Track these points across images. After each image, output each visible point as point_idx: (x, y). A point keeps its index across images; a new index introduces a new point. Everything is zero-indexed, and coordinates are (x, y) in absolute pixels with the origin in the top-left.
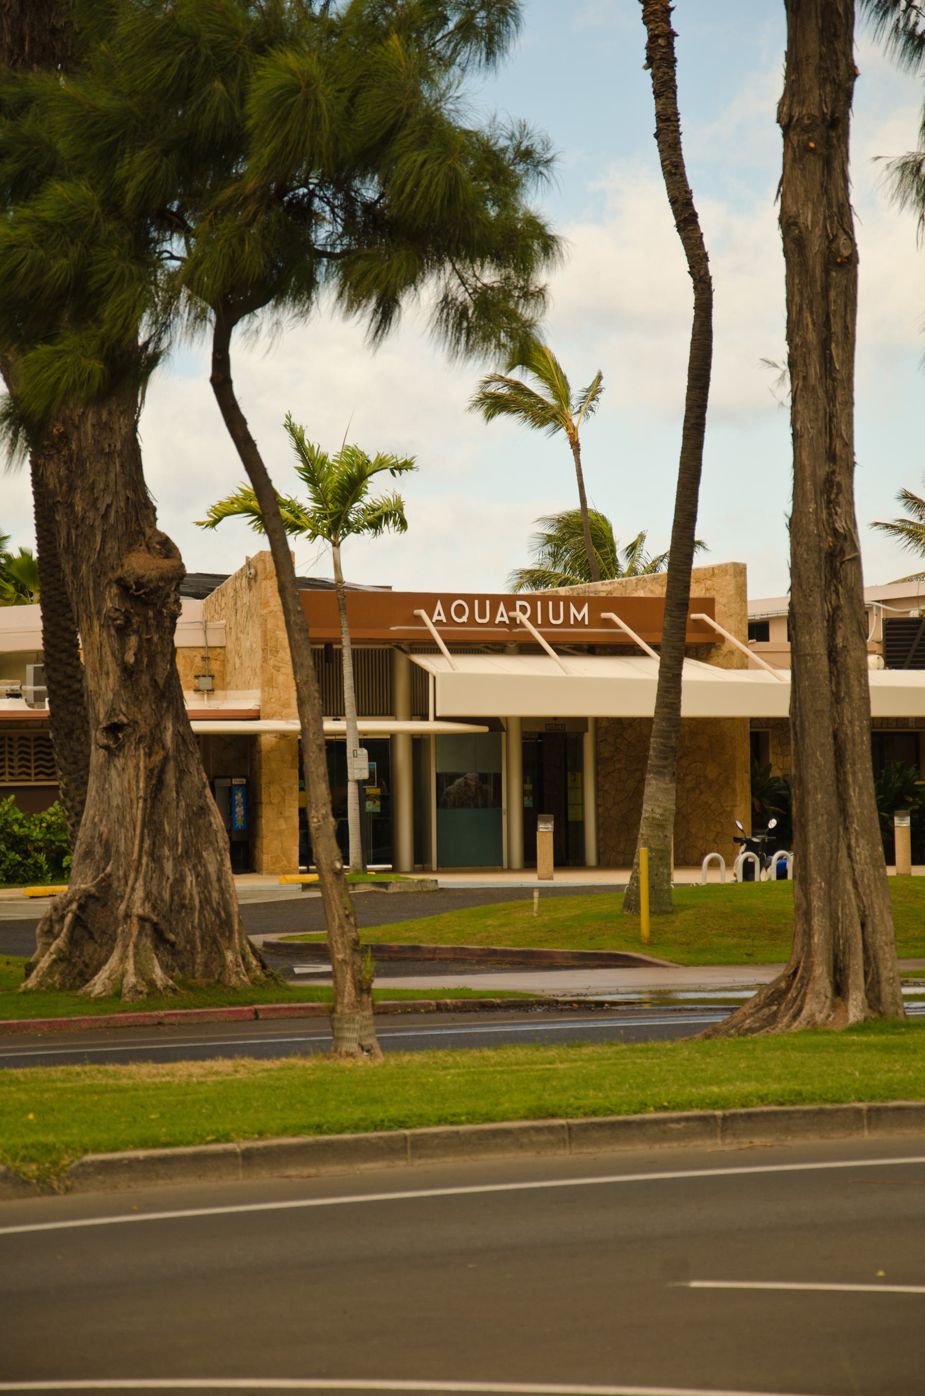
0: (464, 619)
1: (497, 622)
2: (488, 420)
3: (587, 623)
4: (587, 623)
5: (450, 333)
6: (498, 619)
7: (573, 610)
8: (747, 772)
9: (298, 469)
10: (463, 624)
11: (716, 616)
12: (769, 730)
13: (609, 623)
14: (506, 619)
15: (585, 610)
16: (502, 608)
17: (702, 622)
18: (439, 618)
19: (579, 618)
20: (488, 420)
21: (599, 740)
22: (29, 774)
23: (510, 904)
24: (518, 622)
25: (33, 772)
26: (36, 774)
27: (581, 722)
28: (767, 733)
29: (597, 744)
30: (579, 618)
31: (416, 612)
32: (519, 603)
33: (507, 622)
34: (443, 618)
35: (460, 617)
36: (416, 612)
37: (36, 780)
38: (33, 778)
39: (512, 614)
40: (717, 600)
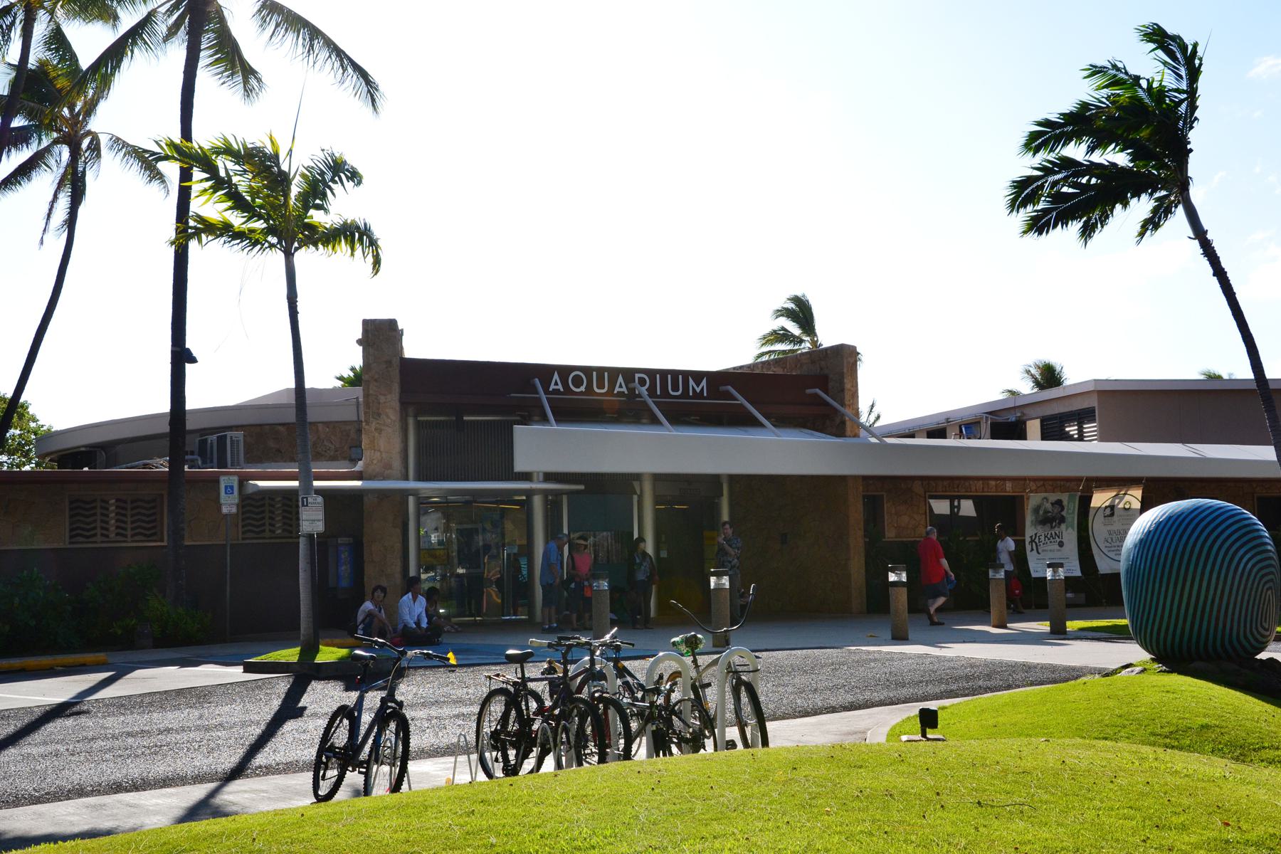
0: (582, 389)
1: (551, 389)
4: (705, 394)
5: (199, 151)
6: (617, 389)
7: (691, 382)
8: (860, 529)
9: (1087, 232)
10: (581, 393)
14: (624, 389)
15: (704, 383)
17: (816, 395)
19: (698, 390)
22: (126, 536)
23: (975, 697)
24: (637, 392)
25: (129, 533)
26: (133, 536)
27: (715, 480)
28: (883, 495)
30: (698, 390)
32: (637, 376)
33: (626, 392)
34: (560, 387)
35: (578, 387)
37: (133, 541)
38: (129, 539)
39: (631, 385)
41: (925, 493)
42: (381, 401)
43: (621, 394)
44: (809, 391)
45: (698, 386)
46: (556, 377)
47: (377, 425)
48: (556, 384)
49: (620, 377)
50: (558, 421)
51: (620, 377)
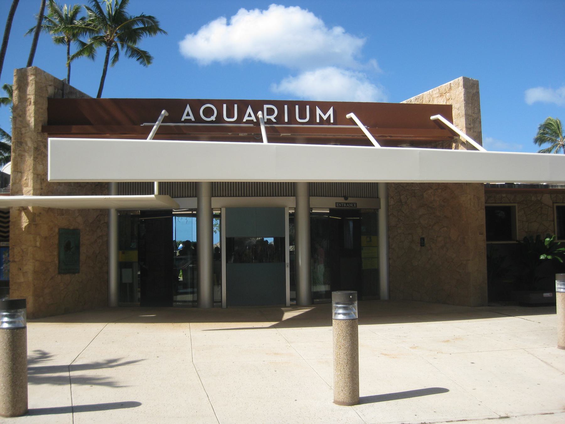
0: (213, 118)
2: (93, 58)
3: (332, 121)
4: (332, 121)
6: (246, 118)
7: (318, 111)
10: (212, 122)
11: (454, 121)
12: (516, 205)
13: (352, 121)
14: (253, 118)
15: (331, 112)
16: (249, 110)
18: (250, 118)
19: (325, 117)
20: (93, 58)
21: (389, 214)
29: (388, 216)
30: (325, 117)
31: (348, 116)
32: (266, 107)
34: (192, 117)
36: (348, 116)
40: (453, 106)
41: (553, 203)
42: (23, 132)
43: (248, 121)
44: (432, 118)
45: (325, 114)
46: (188, 109)
47: (20, 152)
48: (188, 115)
49: (188, 107)
50: (270, 140)
51: (188, 107)
